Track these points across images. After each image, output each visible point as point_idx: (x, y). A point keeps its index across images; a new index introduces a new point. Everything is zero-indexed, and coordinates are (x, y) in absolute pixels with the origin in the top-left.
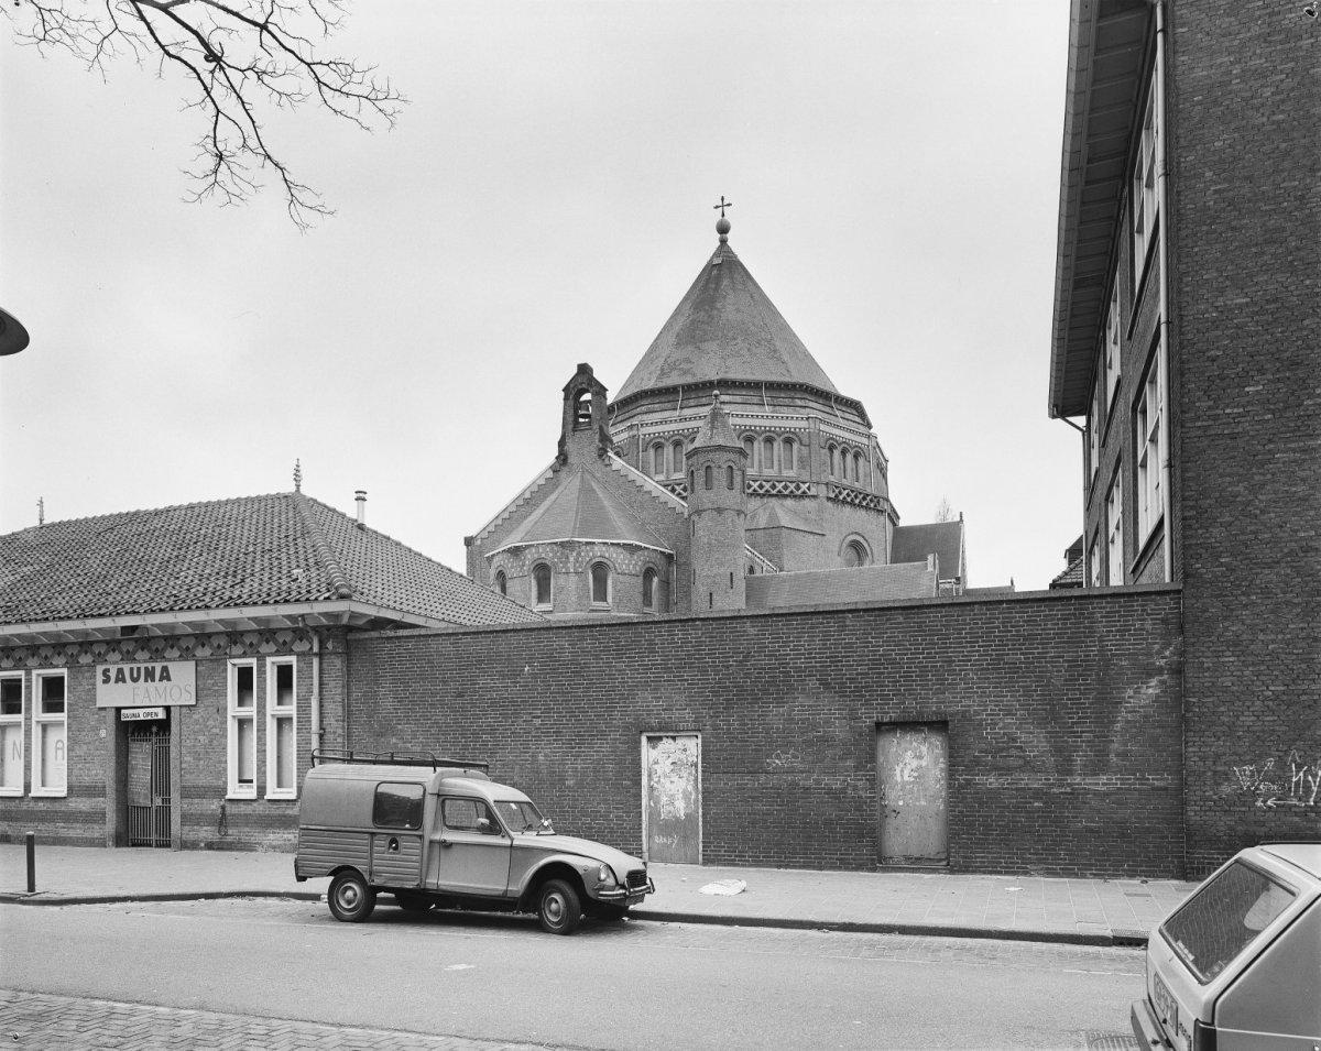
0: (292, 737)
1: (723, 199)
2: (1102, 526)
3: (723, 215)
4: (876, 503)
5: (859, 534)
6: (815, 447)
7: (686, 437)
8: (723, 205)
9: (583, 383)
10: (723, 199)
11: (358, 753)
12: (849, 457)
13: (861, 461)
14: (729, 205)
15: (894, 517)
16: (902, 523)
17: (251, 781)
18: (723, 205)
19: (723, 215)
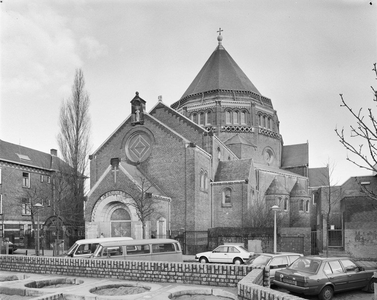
0: (362, 128)
1: (220, 29)
2: (160, 245)
3: (220, 34)
4: (277, 136)
5: (270, 148)
6: (254, 115)
7: (240, 110)
8: (220, 31)
9: (137, 102)
10: (220, 29)
11: (214, 188)
12: (266, 119)
13: (271, 120)
14: (222, 31)
15: (282, 143)
16: (284, 145)
17: (27, 251)
18: (220, 31)
19: (220, 34)
